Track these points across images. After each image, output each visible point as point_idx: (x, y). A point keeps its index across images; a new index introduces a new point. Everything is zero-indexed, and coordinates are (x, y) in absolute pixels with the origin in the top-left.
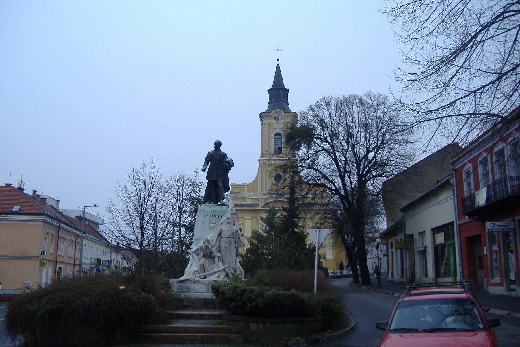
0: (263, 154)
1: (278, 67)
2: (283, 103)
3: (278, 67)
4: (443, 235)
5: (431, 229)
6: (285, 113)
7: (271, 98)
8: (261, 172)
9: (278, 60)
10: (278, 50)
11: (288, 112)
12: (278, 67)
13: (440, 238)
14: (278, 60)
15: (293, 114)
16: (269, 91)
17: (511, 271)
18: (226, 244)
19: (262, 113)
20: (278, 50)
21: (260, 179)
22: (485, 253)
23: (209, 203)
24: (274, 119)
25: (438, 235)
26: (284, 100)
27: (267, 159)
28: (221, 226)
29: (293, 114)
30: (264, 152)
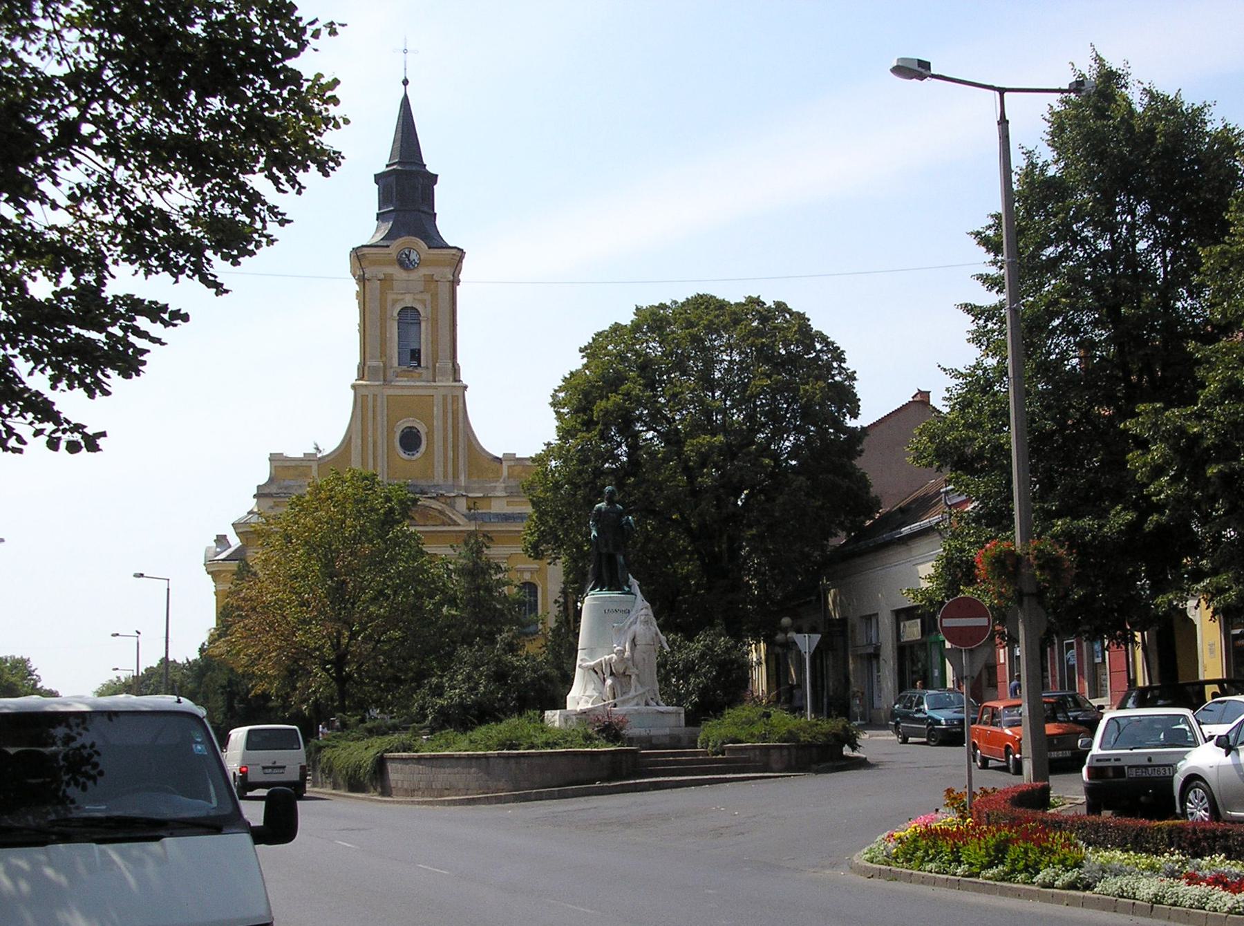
0: (366, 368)
1: (405, 104)
2: (423, 216)
3: (405, 103)
4: (919, 624)
5: (893, 611)
6: (429, 248)
7: (384, 199)
8: (359, 422)
9: (406, 82)
10: (405, 51)
11: (440, 245)
12: (405, 104)
13: (913, 630)
14: (406, 82)
15: (454, 251)
16: (378, 178)
17: (1050, 706)
18: (644, 655)
19: (363, 246)
20: (405, 51)
21: (356, 441)
22: (1002, 661)
23: (601, 590)
24: (397, 267)
25: (908, 623)
26: (426, 209)
27: (377, 383)
28: (633, 628)
29: (454, 251)
30: (368, 363)
